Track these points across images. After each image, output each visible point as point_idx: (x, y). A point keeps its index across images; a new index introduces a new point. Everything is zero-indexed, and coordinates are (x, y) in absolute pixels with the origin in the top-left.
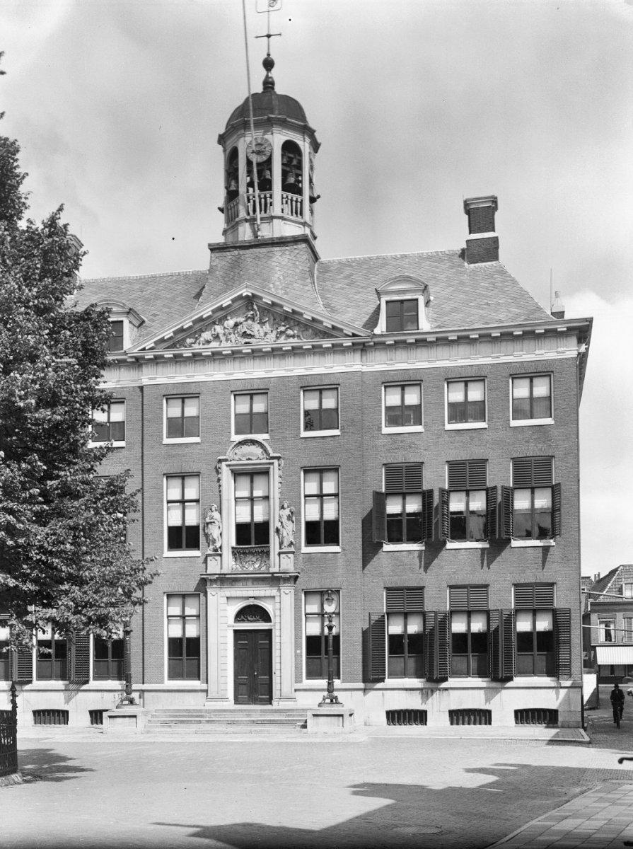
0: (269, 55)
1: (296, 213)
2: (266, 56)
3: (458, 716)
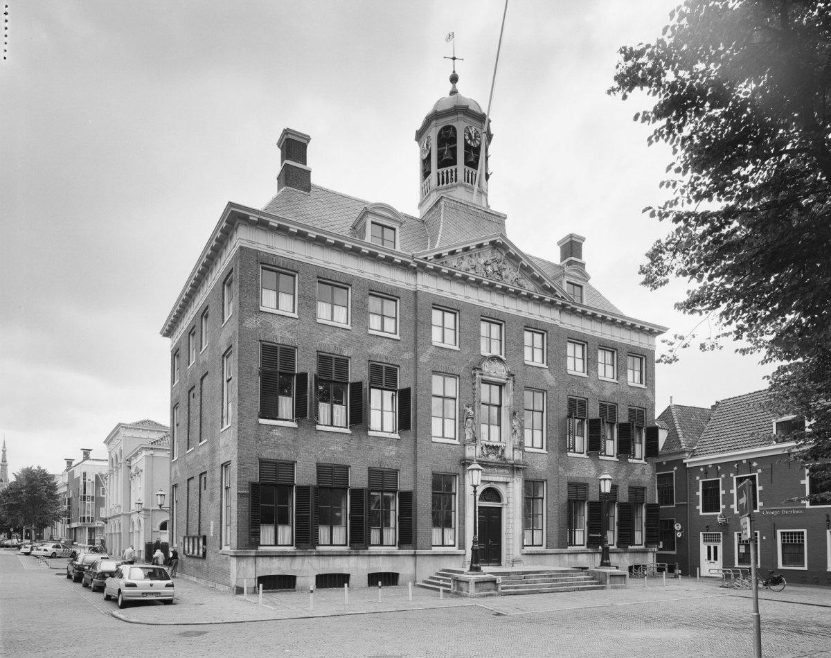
0: (454, 72)
1: (468, 181)
2: (452, 73)
3: (375, 579)
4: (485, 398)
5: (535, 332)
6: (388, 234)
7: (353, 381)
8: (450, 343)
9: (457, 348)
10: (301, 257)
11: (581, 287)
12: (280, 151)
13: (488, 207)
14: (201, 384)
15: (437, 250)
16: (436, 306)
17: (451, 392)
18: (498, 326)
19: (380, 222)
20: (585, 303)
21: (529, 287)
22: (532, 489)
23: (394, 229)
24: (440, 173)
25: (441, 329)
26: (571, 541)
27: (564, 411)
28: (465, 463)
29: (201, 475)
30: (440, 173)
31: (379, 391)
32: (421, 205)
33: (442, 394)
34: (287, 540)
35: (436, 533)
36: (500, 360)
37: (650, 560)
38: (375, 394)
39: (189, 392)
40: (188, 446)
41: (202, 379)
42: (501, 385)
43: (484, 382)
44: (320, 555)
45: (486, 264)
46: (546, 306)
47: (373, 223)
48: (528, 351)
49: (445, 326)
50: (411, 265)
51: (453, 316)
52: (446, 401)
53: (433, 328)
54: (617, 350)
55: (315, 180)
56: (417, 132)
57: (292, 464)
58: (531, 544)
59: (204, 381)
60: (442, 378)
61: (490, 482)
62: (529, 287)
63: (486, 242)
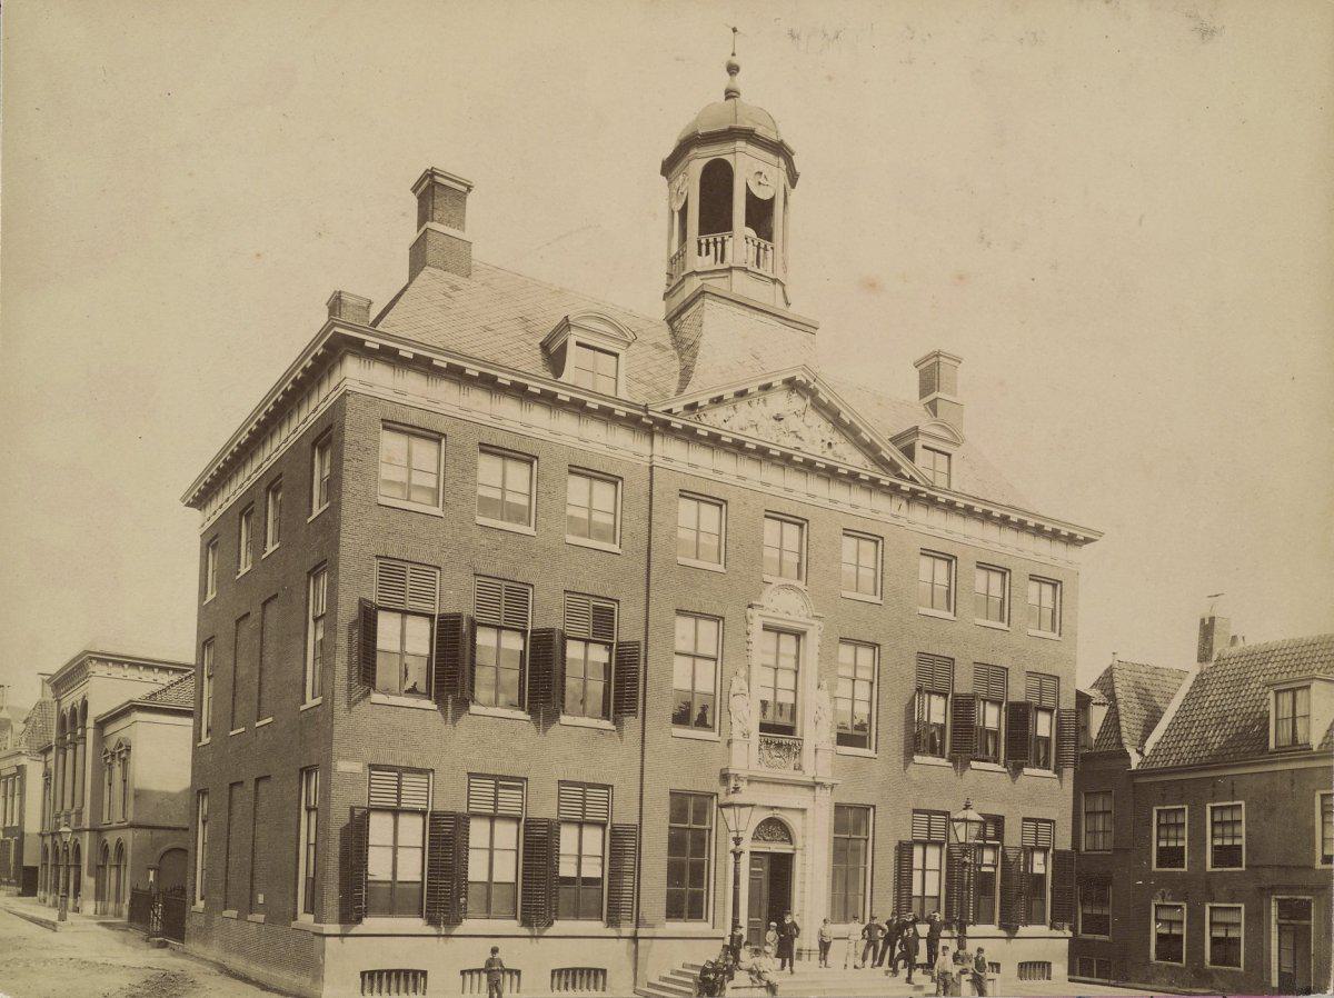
5: (786, 521)
11: (949, 455)
18: (873, 544)
20: (954, 487)
21: (854, 460)
23: (617, 355)
24: (703, 241)
30: (703, 241)
33: (698, 661)
46: (843, 483)
49: (785, 547)
56: (663, 162)
60: (852, 647)
61: (772, 808)
62: (854, 460)
63: (777, 382)
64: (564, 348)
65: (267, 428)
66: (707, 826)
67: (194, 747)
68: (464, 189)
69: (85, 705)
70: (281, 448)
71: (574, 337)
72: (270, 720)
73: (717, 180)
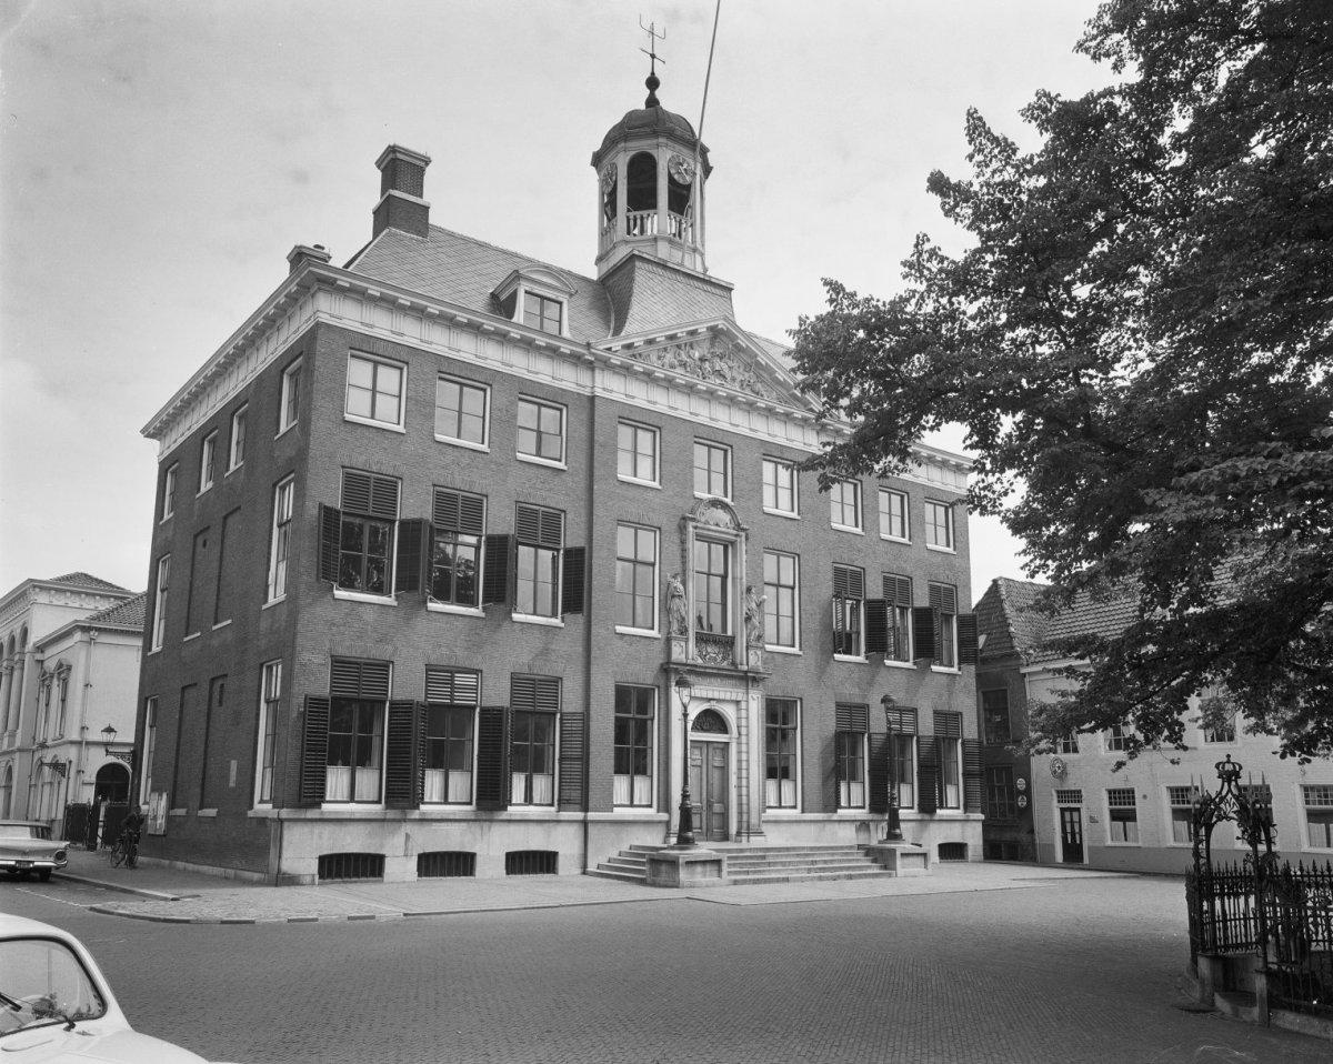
0: (653, 73)
2: (649, 75)
4: (770, 575)
6: (552, 310)
7: (570, 545)
8: (644, 477)
9: (656, 484)
10: (496, 364)
12: (379, 173)
13: (706, 270)
14: (224, 527)
15: (627, 337)
16: (623, 420)
17: (647, 553)
19: (540, 293)
22: (779, 716)
23: (560, 303)
24: (632, 217)
25: (378, 389)
26: (941, 802)
27: (826, 588)
28: (667, 669)
29: (213, 680)
30: (632, 217)
31: (532, 549)
32: (600, 260)
33: (780, 589)
34: (856, 799)
35: (621, 784)
36: (725, 506)
37: (973, 836)
38: (525, 552)
39: (196, 536)
40: (187, 628)
41: (225, 518)
42: (727, 545)
43: (700, 538)
44: (423, 820)
45: (702, 360)
47: (526, 292)
48: (768, 493)
50: (587, 357)
51: (650, 435)
52: (640, 568)
53: (881, 514)
54: (731, 447)
55: (434, 219)
57: (383, 667)
58: (777, 805)
59: (231, 521)
61: (710, 700)
64: (513, 297)
65: (253, 342)
66: (648, 716)
67: (144, 656)
68: (422, 164)
69: (25, 632)
70: (290, 339)
71: (523, 287)
72: (229, 622)
73: (642, 169)
